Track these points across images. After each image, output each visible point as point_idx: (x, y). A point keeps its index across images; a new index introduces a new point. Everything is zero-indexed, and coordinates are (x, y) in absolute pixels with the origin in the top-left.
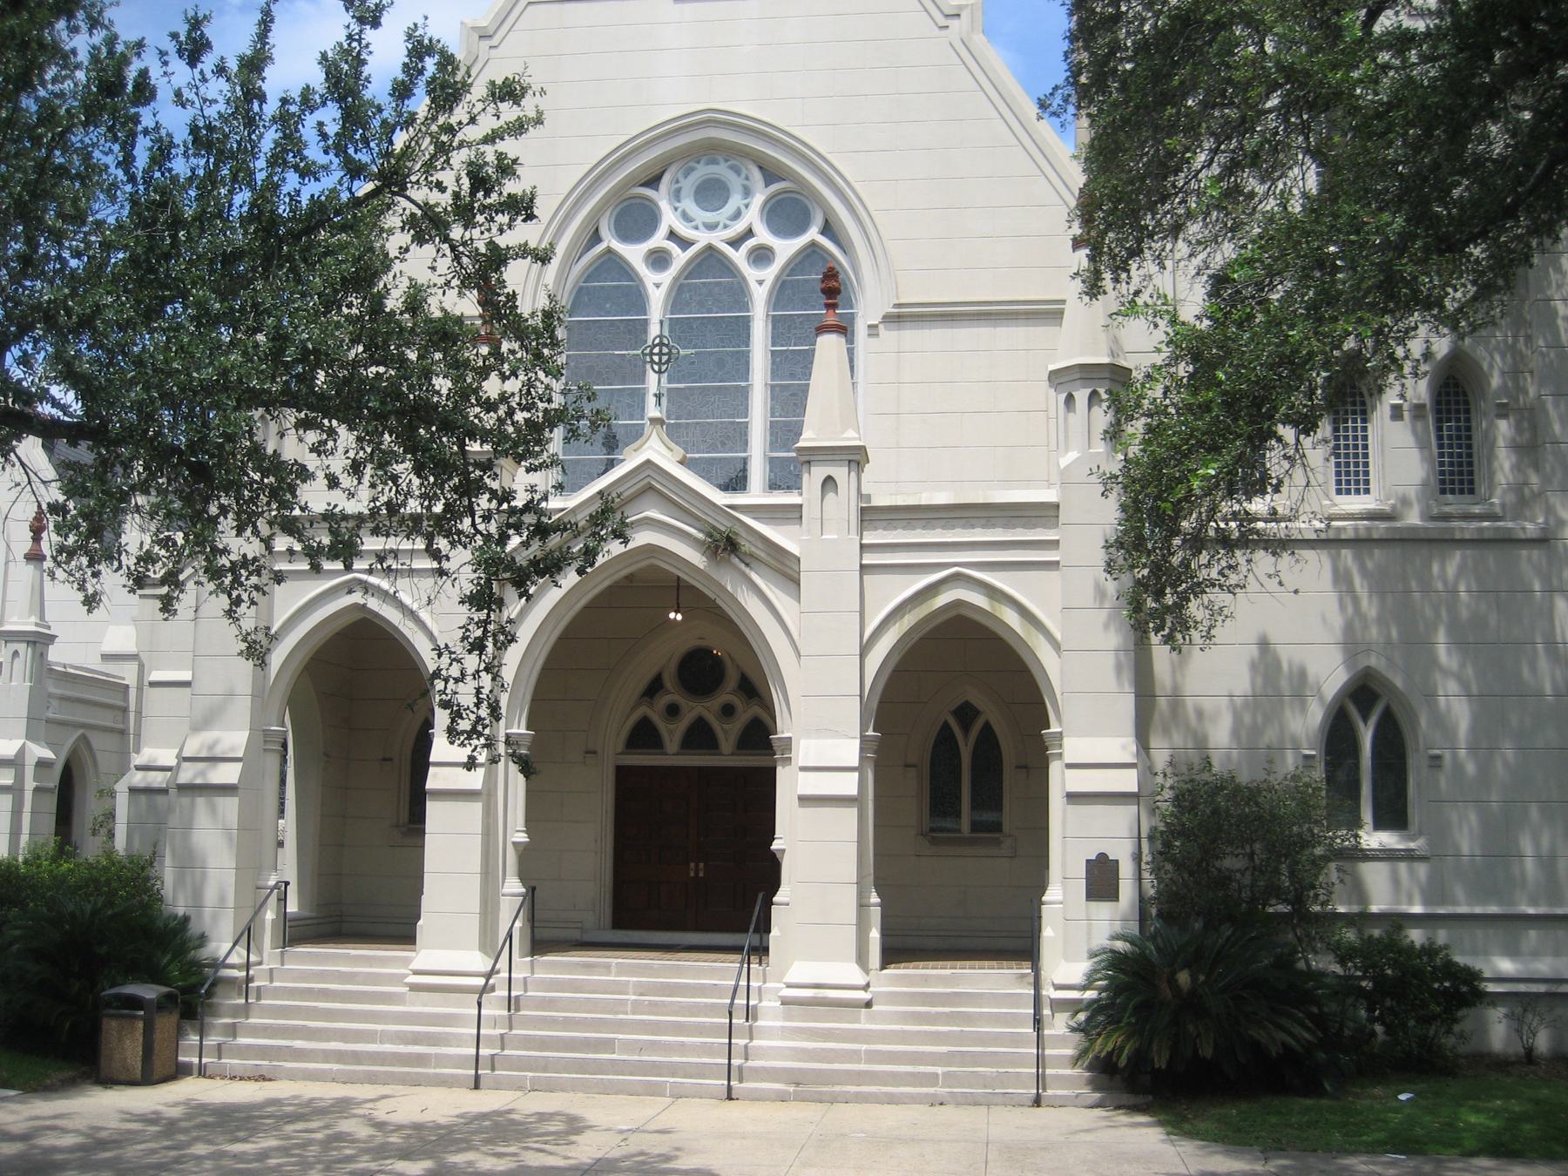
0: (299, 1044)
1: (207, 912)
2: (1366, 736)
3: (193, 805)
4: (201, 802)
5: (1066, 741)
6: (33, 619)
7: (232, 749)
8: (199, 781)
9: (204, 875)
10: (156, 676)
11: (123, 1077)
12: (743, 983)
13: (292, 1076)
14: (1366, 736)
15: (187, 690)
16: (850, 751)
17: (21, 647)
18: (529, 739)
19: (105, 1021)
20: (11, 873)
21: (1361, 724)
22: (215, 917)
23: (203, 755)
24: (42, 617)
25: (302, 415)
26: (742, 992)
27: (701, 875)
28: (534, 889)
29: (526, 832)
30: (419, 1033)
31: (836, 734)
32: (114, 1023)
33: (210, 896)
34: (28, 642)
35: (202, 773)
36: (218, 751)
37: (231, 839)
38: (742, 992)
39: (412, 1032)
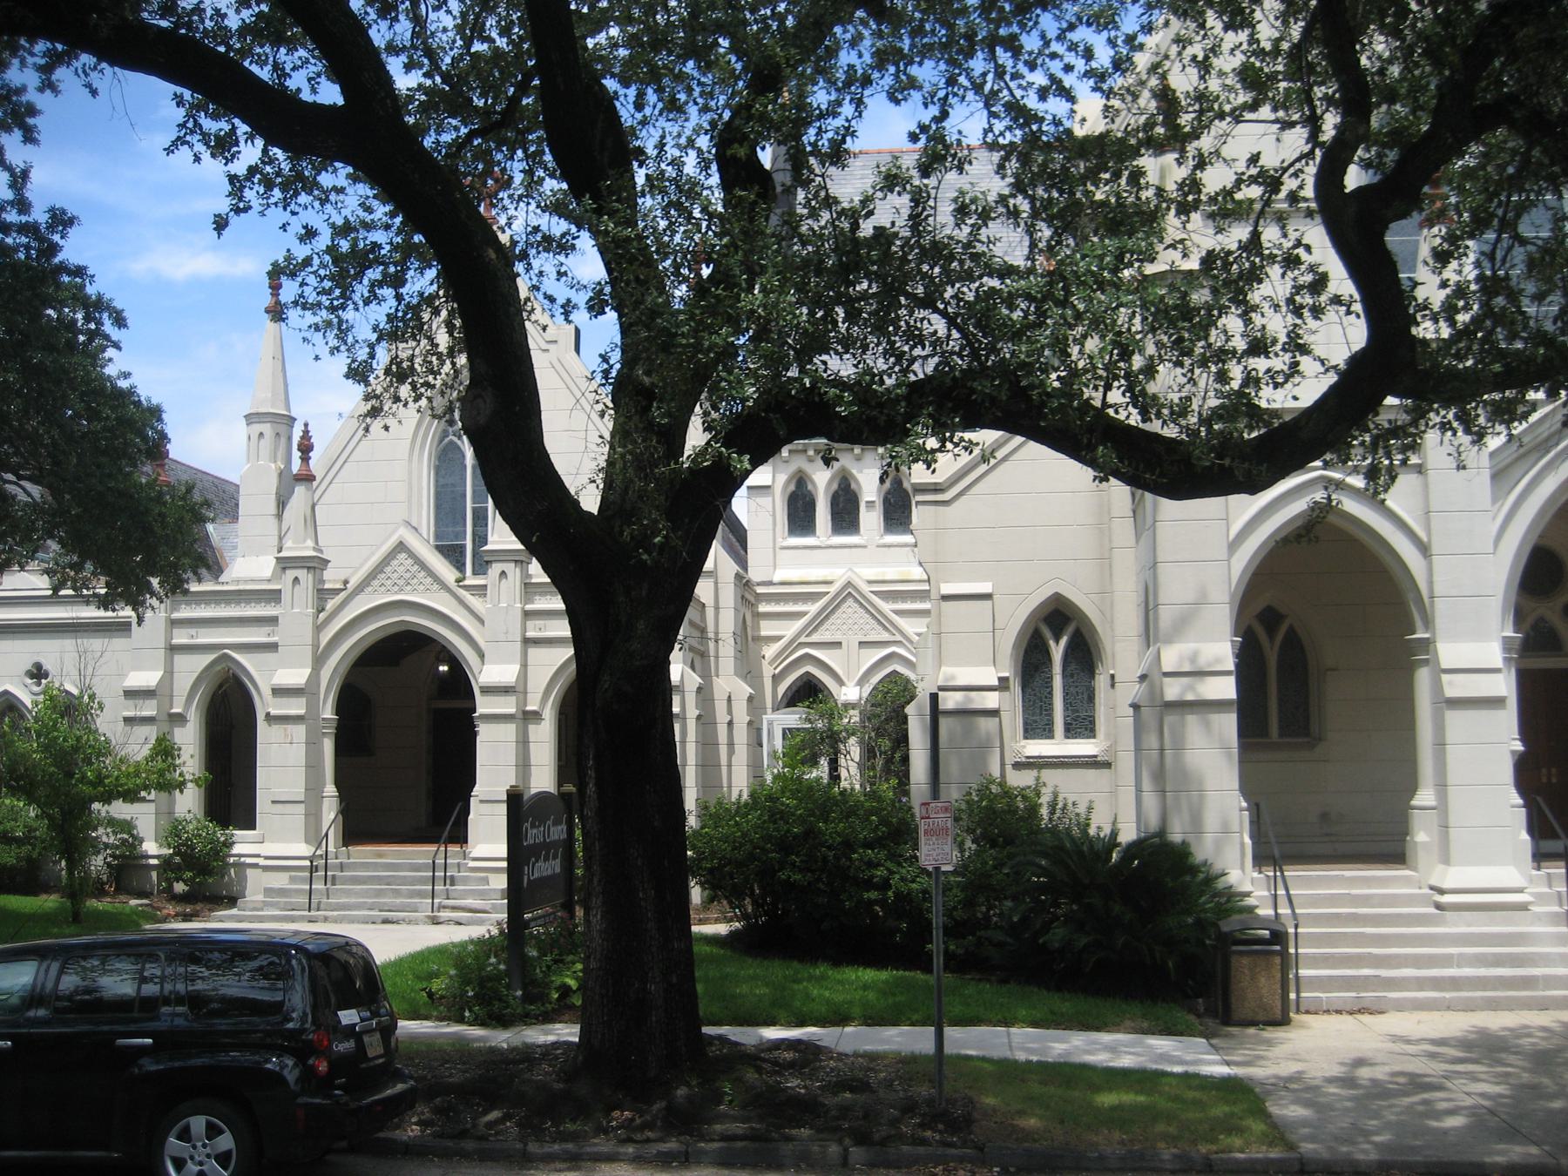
0: (1384, 973)
1: (1209, 839)
2: (1057, 651)
3: (1183, 725)
4: (1192, 721)
5: (1439, 645)
6: (310, 543)
7: (1218, 660)
8: (1190, 697)
9: (1201, 798)
10: (947, 589)
11: (1261, 1017)
12: (1281, 892)
13: (1400, 1006)
14: (1057, 651)
15: (988, 603)
16: (1494, 654)
17: (302, 574)
18: (1518, 642)
19: (1234, 960)
20: (992, 799)
21: (1052, 643)
22: (1219, 846)
23: (1187, 668)
24: (317, 543)
25: (1473, 287)
26: (1282, 901)
27: (1554, 780)
28: (1257, 805)
29: (1521, 740)
30: (1500, 954)
31: (509, 662)
32: (1245, 961)
33: (1211, 821)
34: (309, 568)
35: (1191, 688)
36: (1203, 663)
37: (1229, 755)
38: (1282, 901)
39: (1494, 955)
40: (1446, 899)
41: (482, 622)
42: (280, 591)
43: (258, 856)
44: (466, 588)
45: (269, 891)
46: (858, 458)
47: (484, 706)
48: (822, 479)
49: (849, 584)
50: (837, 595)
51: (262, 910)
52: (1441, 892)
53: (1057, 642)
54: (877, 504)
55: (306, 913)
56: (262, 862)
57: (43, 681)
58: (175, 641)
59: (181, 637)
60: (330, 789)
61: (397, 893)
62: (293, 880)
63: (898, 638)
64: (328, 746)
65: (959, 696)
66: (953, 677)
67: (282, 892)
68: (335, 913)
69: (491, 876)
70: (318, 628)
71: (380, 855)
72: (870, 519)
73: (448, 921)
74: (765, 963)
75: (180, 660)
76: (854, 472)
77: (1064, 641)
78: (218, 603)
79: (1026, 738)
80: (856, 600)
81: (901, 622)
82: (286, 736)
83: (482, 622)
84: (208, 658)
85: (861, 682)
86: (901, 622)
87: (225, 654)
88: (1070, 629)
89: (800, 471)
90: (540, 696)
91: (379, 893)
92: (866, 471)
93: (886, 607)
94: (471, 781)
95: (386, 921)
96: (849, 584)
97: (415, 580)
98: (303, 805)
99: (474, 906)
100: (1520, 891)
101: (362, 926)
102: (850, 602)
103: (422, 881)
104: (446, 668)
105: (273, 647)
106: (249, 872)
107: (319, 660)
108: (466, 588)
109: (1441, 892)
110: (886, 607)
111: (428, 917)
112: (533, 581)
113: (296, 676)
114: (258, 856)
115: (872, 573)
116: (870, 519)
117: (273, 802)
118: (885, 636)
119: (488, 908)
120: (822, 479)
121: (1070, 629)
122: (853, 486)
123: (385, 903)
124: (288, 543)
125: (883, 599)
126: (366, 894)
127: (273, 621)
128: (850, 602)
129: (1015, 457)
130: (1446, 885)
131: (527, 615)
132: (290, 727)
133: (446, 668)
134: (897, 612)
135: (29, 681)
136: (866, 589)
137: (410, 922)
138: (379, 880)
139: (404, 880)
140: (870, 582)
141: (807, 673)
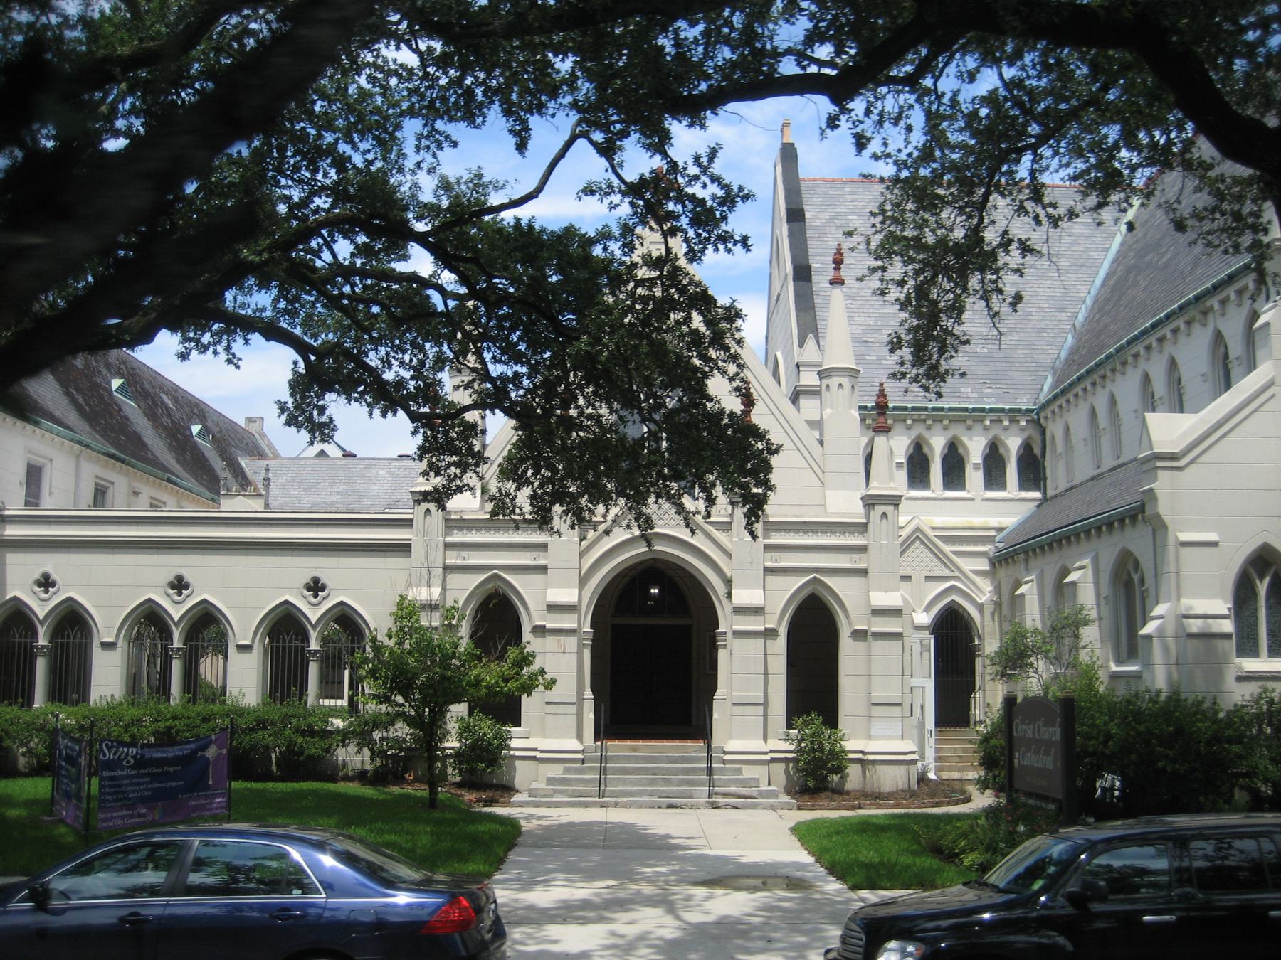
21: (1258, 582)
40: (727, 757)
41: (729, 555)
42: (411, 520)
43: (535, 750)
44: (712, 524)
45: (550, 781)
46: (969, 428)
47: (727, 623)
48: (937, 444)
49: (918, 529)
50: (909, 537)
51: (552, 796)
52: (725, 753)
53: (1261, 581)
54: (905, 465)
55: (597, 799)
56: (539, 755)
57: (51, 589)
58: (448, 562)
59: (453, 559)
60: (588, 693)
61: (668, 782)
62: (567, 770)
63: (957, 574)
64: (587, 654)
65: (1199, 622)
66: (1191, 608)
67: (563, 781)
68: (625, 799)
69: (744, 768)
70: (582, 554)
71: (635, 749)
72: (974, 477)
73: (726, 806)
74: (9, 792)
75: (455, 579)
76: (965, 439)
77: (1267, 580)
78: (806, 532)
79: (1269, 657)
80: (923, 543)
81: (959, 561)
82: (559, 646)
83: (729, 555)
84: (482, 577)
85: (927, 610)
86: (959, 561)
87: (496, 574)
88: (1271, 572)
89: (955, 437)
90: (777, 615)
91: (652, 782)
92: (975, 438)
93: (948, 549)
94: (714, 687)
95: (670, 806)
96: (918, 529)
97: (667, 516)
98: (574, 706)
99: (742, 793)
100: (914, 753)
101: (649, 810)
102: (918, 543)
103: (722, 771)
104: (652, 591)
105: (544, 569)
106: (518, 763)
107: (583, 582)
108: (712, 524)
109: (725, 753)
110: (948, 549)
111: (708, 802)
112: (770, 519)
113: (568, 595)
114: (535, 750)
115: (939, 521)
116: (974, 477)
117: (547, 703)
118: (946, 572)
119: (754, 795)
120: (937, 444)
121: (1271, 572)
122: (961, 450)
123: (663, 791)
124: (873, 484)
125: (944, 542)
126: (640, 782)
127: (863, 549)
128: (918, 543)
129: (1231, 435)
130: (867, 750)
131: (448, 546)
132: (563, 639)
133: (652, 591)
134: (957, 553)
135: (171, 592)
136: (931, 534)
137: (692, 807)
138: (653, 771)
139: (677, 772)
140: (933, 528)
141: (953, 601)
